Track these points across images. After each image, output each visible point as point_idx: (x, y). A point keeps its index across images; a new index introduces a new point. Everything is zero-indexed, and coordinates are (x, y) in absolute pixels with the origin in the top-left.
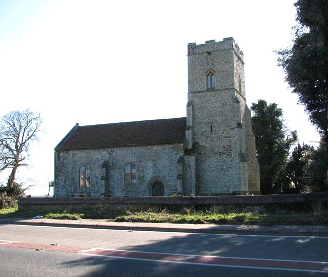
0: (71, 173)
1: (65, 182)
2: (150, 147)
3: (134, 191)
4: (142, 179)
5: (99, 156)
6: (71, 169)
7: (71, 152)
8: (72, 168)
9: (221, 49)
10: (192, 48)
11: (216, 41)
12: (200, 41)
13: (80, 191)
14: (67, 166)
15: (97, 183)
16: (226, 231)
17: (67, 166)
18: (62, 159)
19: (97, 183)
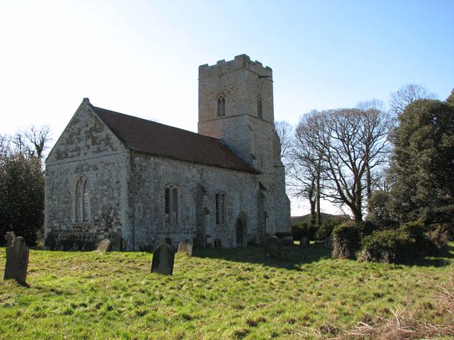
0: (153, 197)
1: (145, 213)
2: (235, 172)
3: (224, 231)
4: (231, 216)
5: (189, 175)
6: (152, 191)
7: (152, 158)
8: (155, 189)
9: (136, 228)
10: (204, 70)
11: (226, 61)
12: (212, 63)
13: (167, 231)
14: (147, 184)
15: (187, 218)
16: (261, 105)
17: (147, 184)
18: (138, 169)
19: (187, 218)
